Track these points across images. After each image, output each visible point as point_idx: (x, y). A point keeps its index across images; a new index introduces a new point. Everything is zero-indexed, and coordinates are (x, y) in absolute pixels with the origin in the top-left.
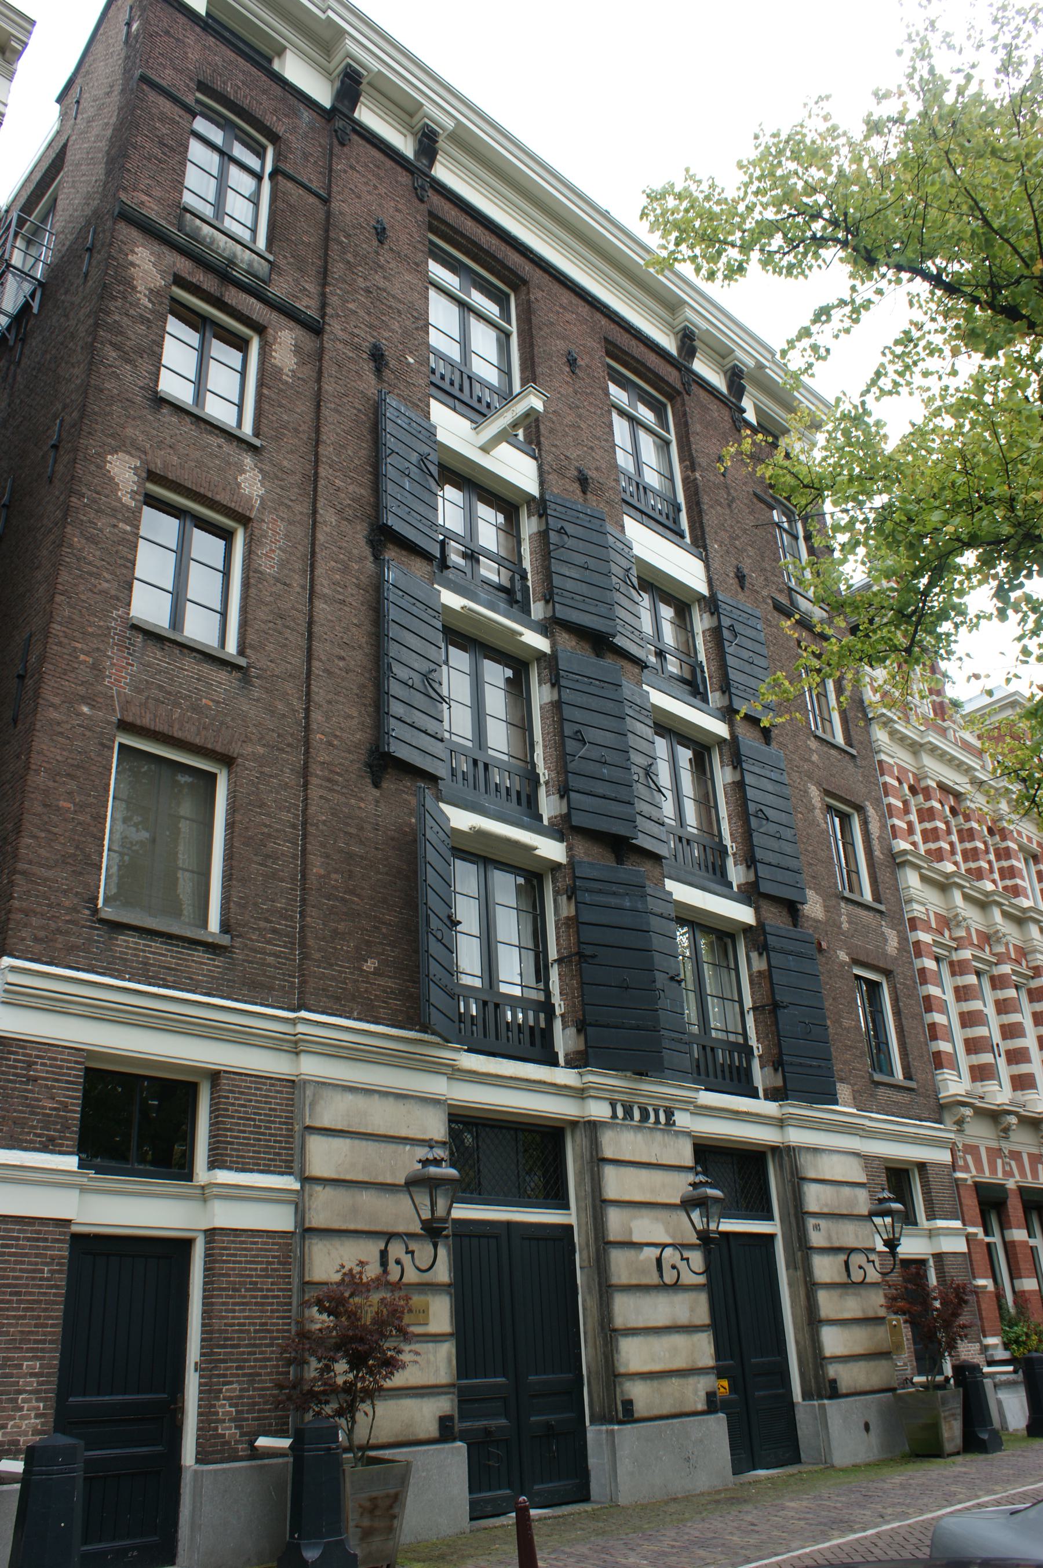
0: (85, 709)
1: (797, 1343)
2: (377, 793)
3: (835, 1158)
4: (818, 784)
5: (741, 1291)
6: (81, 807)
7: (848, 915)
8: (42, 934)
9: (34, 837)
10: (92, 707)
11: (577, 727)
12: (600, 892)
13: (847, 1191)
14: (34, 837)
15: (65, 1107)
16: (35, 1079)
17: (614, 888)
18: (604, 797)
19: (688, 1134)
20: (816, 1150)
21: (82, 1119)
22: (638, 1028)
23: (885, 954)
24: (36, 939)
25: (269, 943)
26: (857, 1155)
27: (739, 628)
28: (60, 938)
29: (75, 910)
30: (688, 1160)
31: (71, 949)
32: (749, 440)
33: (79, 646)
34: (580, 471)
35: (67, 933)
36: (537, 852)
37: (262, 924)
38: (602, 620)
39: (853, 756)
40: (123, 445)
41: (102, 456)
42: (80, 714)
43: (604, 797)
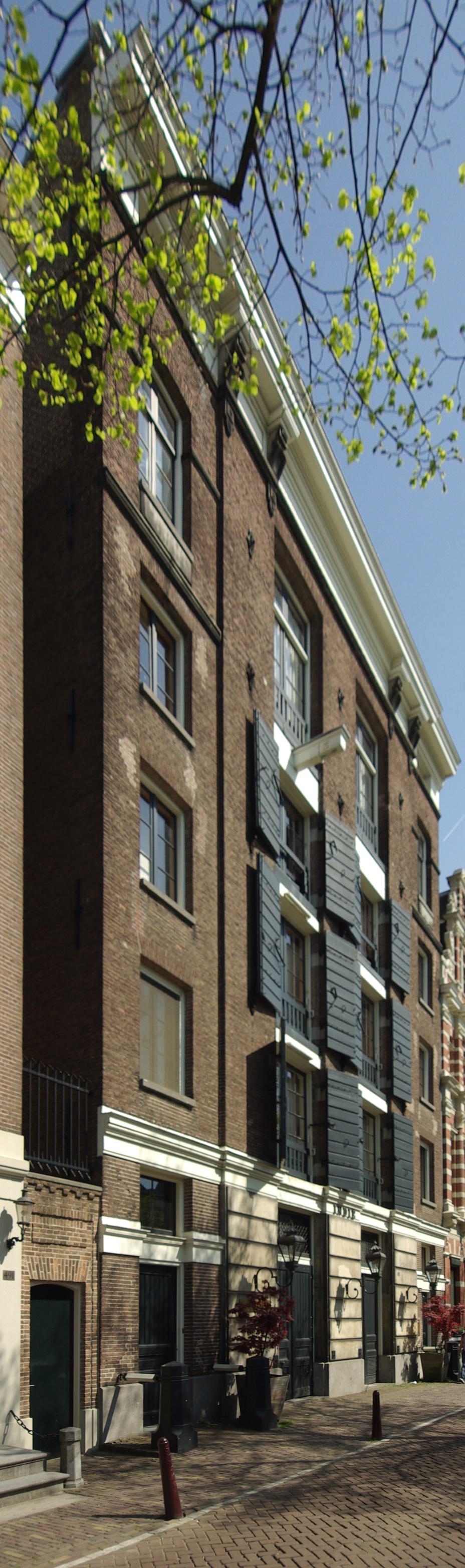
0: (125, 945)
1: (384, 1328)
2: (252, 1018)
3: (408, 1240)
4: (417, 1032)
5: (380, 1291)
6: (129, 1012)
7: (422, 1111)
8: (117, 1093)
9: (109, 1030)
10: (129, 944)
11: (333, 986)
12: (338, 1088)
13: (410, 1256)
14: (109, 1030)
15: (133, 1194)
16: (120, 1179)
17: (344, 1087)
18: (342, 1031)
19: (360, 1223)
20: (402, 1236)
21: (141, 1203)
22: (350, 1167)
23: (432, 1134)
24: (116, 1097)
25: (209, 1105)
26: (414, 1239)
27: (400, 926)
28: (126, 1097)
29: (130, 1079)
30: (359, 1237)
31: (130, 1103)
32: (21, 176)
33: (118, 896)
34: (340, 797)
35: (127, 1093)
36: (311, 1062)
37: (206, 1094)
38: (348, 914)
39: (432, 1016)
40: (126, 732)
41: (116, 737)
42: (123, 948)
43: (342, 1031)
